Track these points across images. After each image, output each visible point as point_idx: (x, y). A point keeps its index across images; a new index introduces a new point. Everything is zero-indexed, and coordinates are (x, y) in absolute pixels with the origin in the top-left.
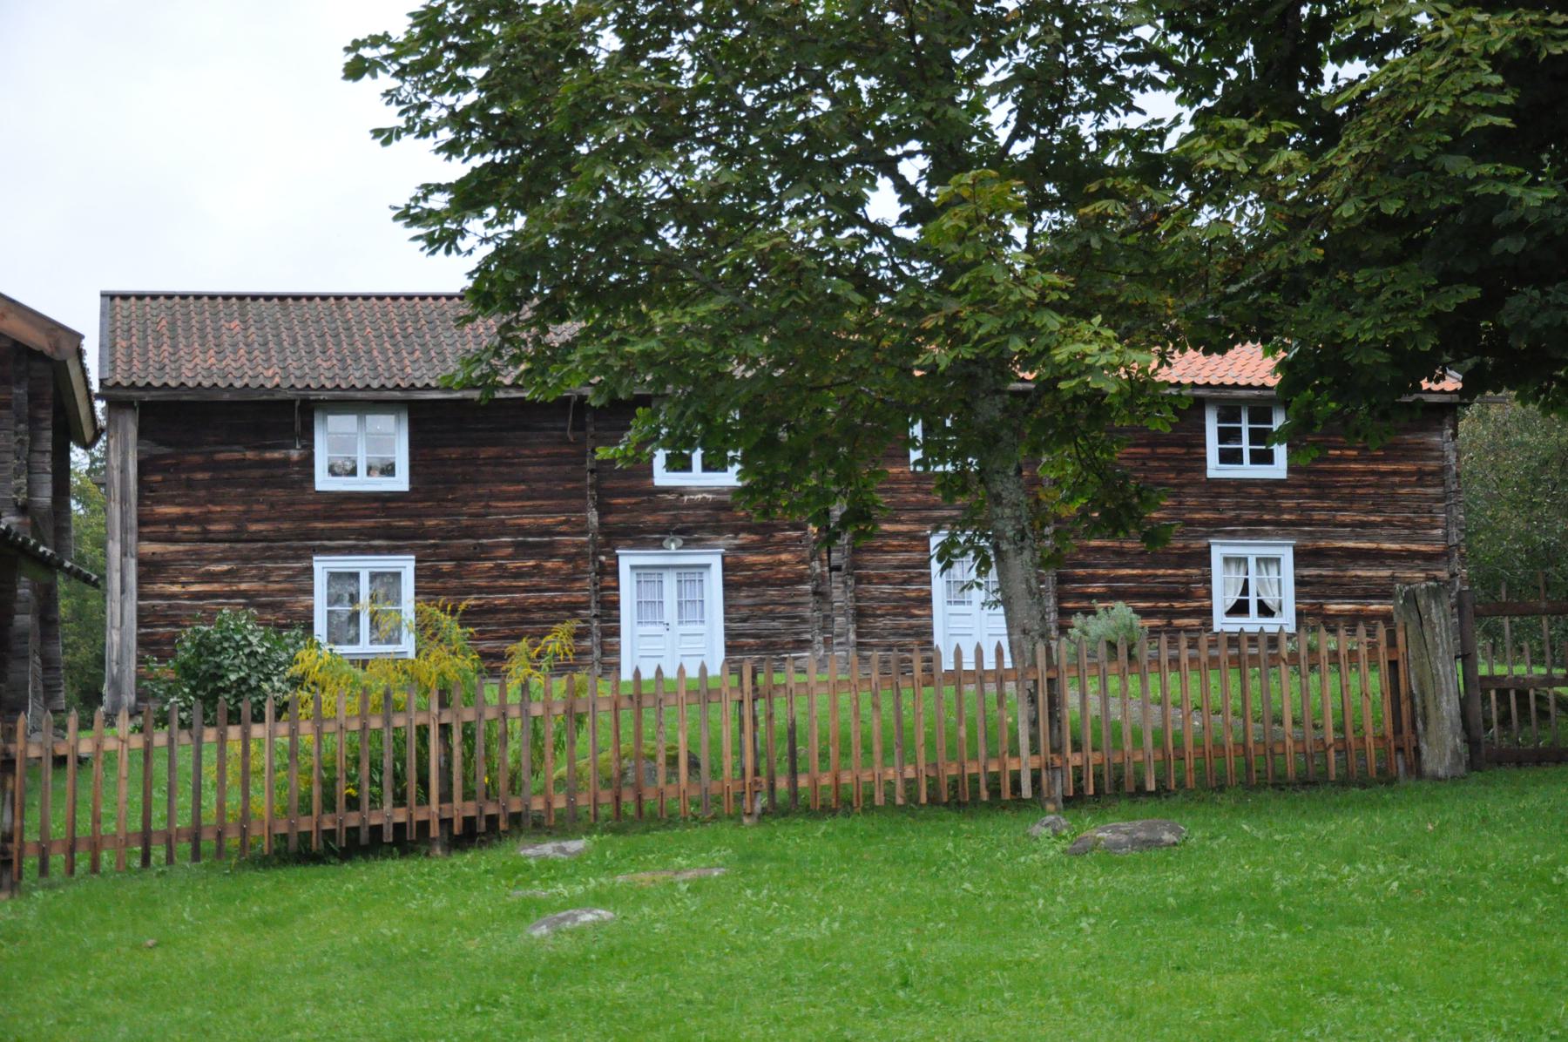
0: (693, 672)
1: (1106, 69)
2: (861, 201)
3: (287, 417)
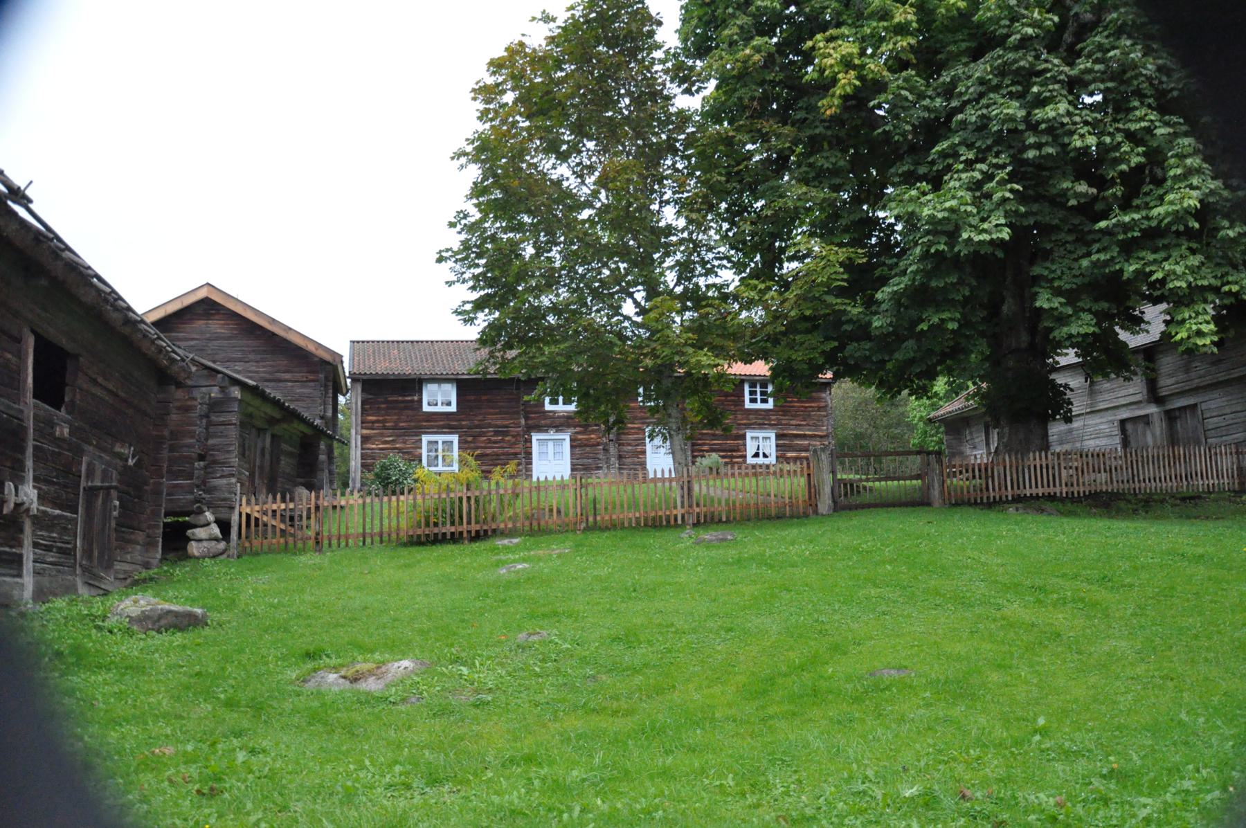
0: (558, 478)
1: (708, 262)
2: (620, 307)
3: (412, 385)
